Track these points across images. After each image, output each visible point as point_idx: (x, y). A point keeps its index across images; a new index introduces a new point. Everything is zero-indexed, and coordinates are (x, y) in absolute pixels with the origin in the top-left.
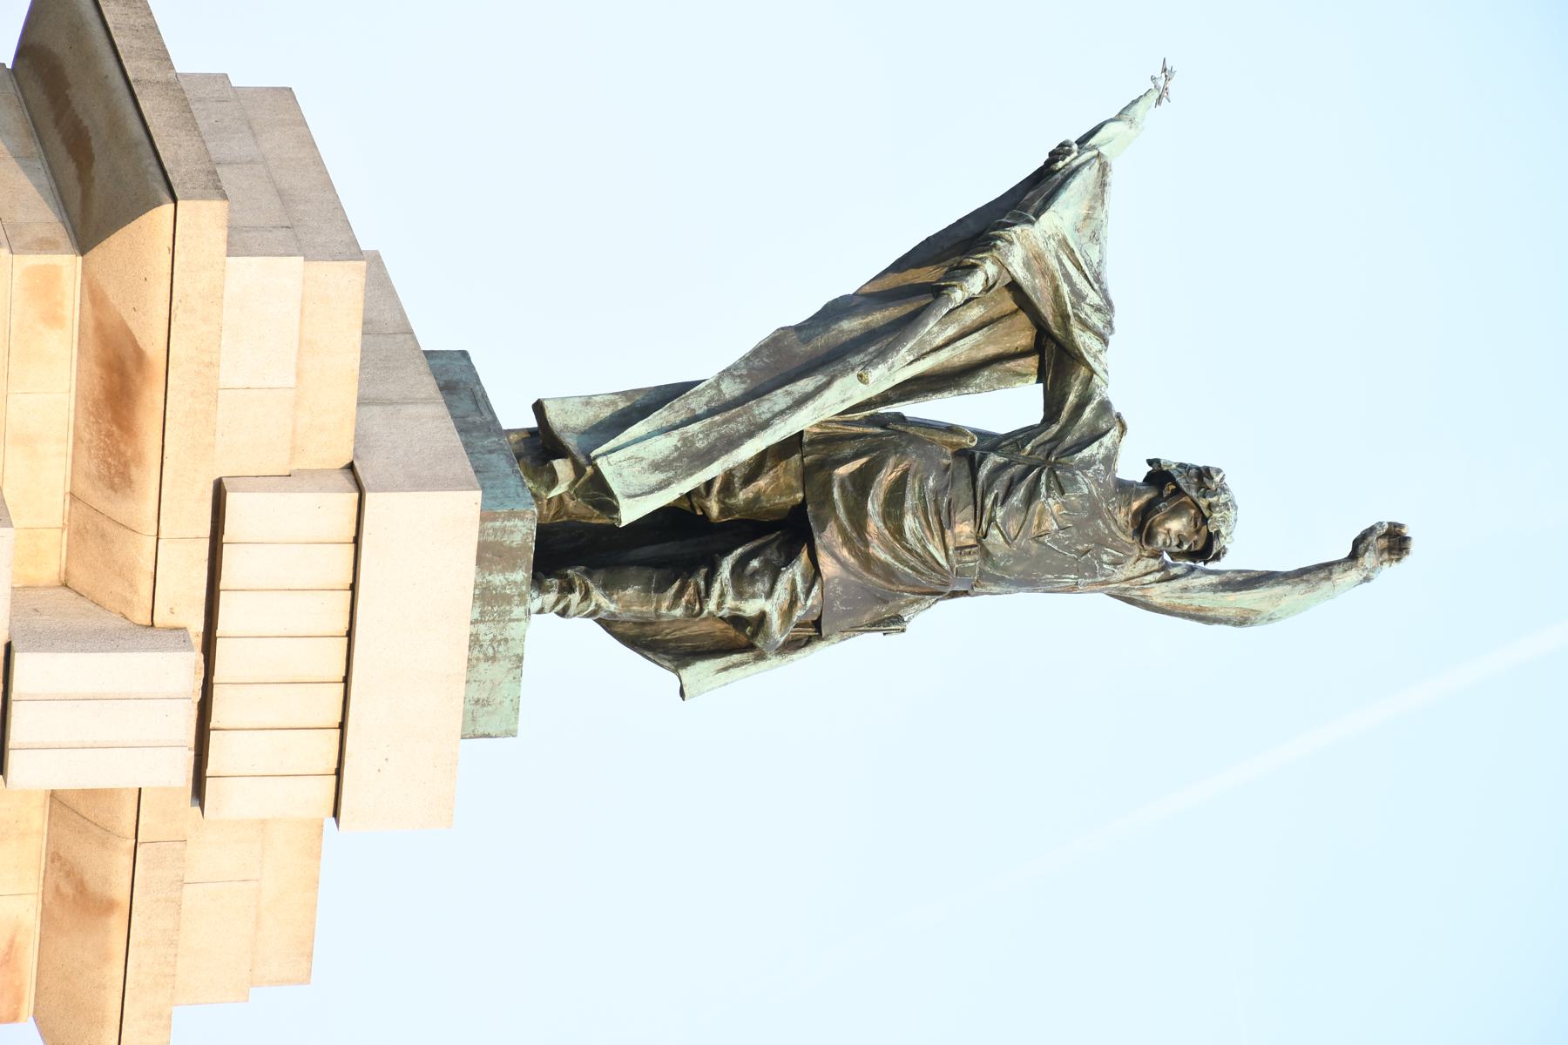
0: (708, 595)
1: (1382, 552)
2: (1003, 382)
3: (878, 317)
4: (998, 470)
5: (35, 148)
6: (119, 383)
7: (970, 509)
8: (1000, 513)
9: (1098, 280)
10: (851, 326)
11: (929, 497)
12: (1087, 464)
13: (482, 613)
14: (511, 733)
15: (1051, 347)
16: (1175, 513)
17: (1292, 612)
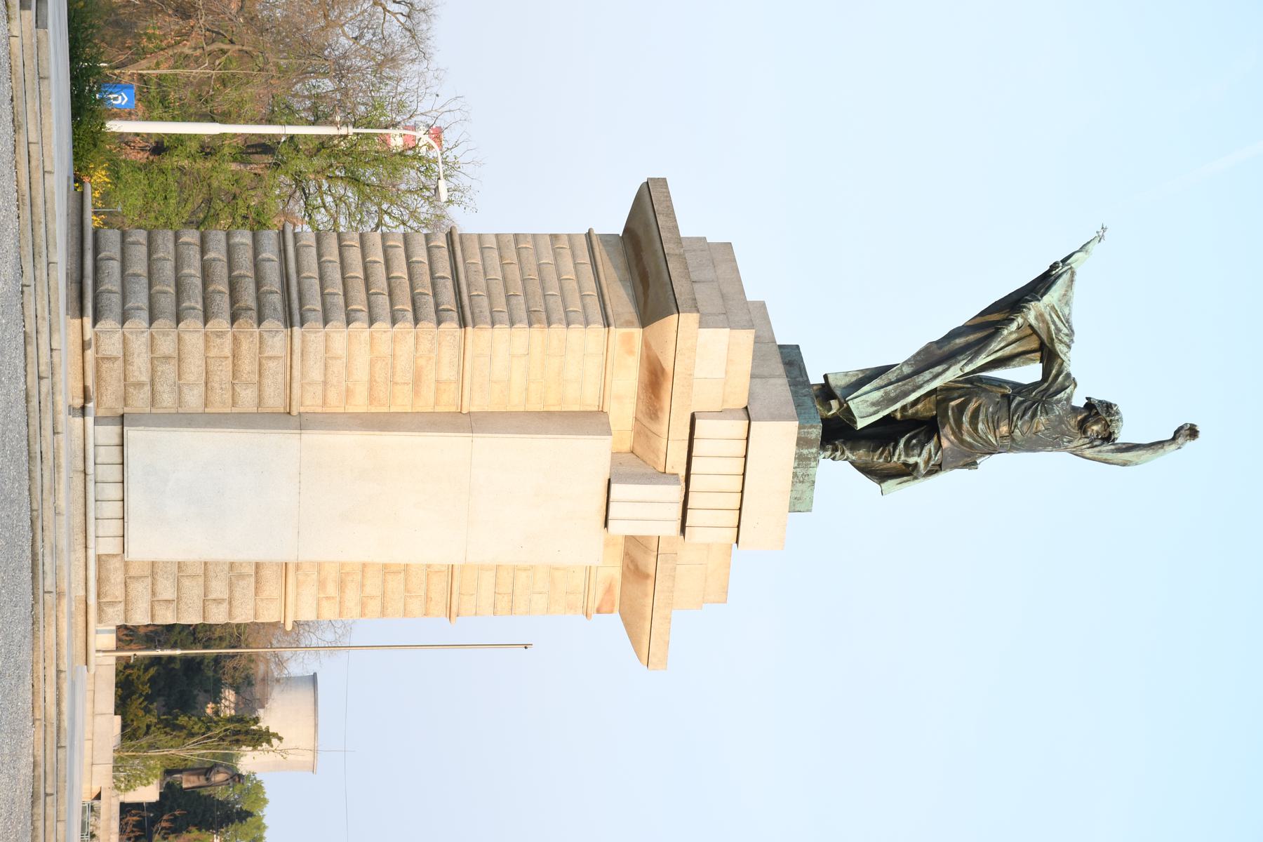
2: (1024, 363)
3: (972, 338)
4: (1020, 403)
5: (628, 276)
8: (1019, 423)
10: (960, 341)
12: (1059, 401)
14: (810, 511)
16: (1096, 423)
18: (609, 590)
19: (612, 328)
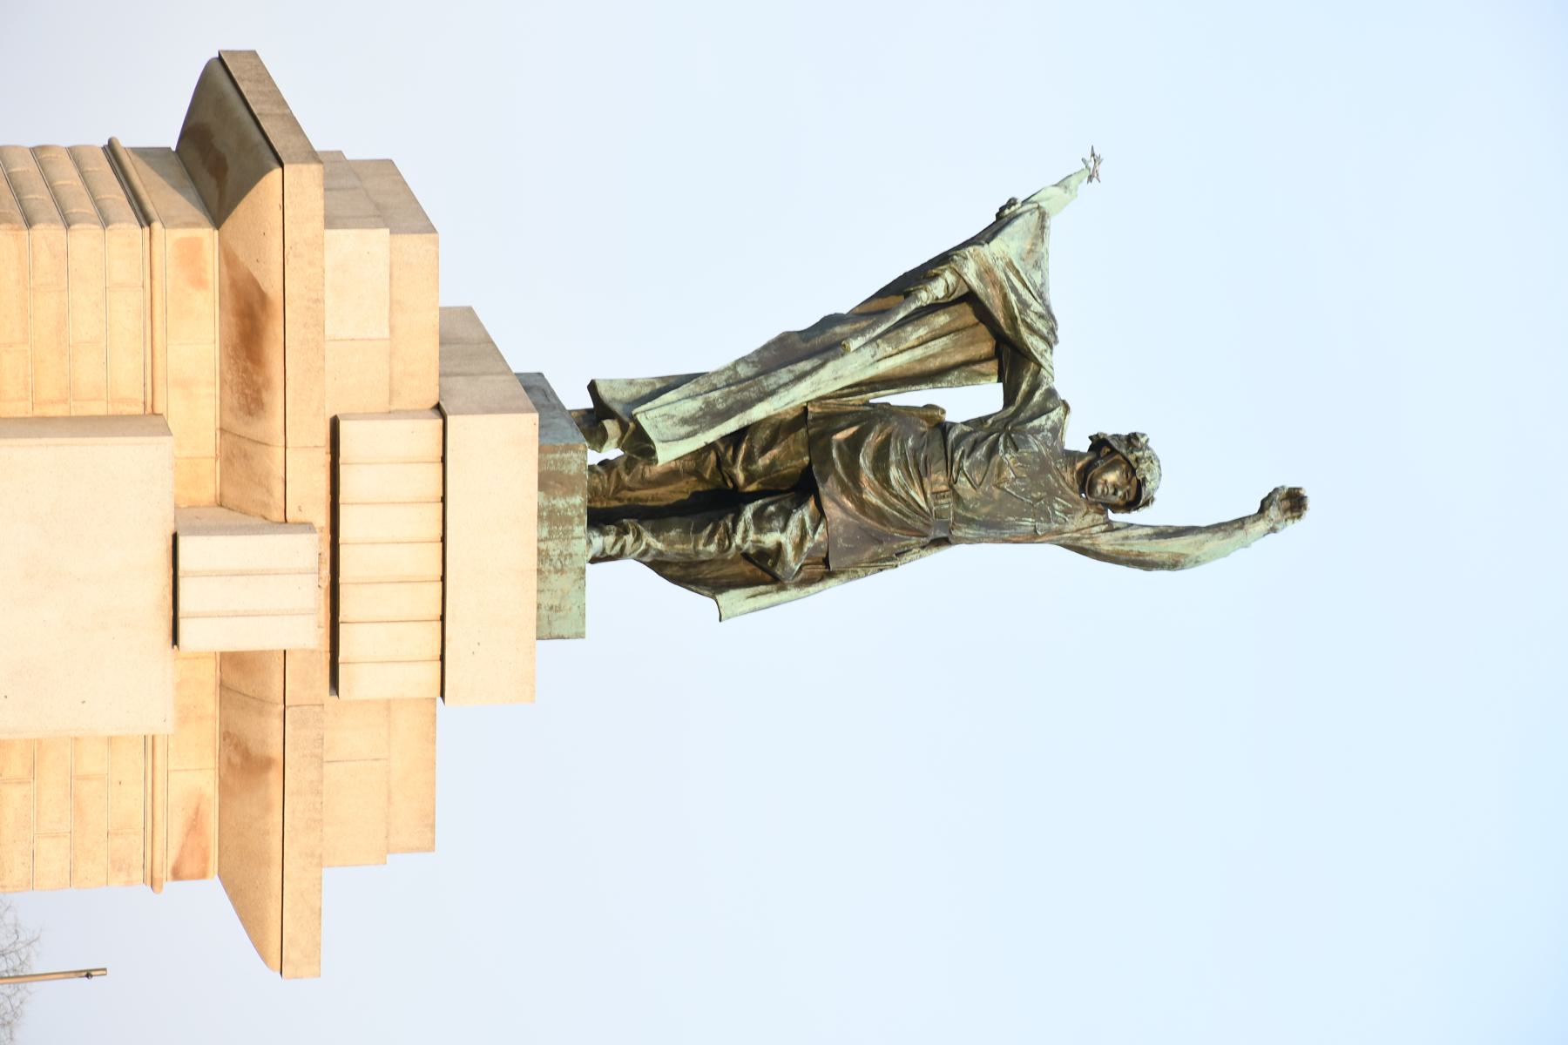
0: (734, 531)
1: (1285, 511)
5: (188, 183)
6: (250, 322)
7: (942, 463)
8: (966, 464)
9: (1041, 296)
12: (1038, 430)
13: (550, 532)
15: (1007, 350)
16: (1110, 467)
17: (1214, 556)
18: (195, 825)
19: (157, 225)
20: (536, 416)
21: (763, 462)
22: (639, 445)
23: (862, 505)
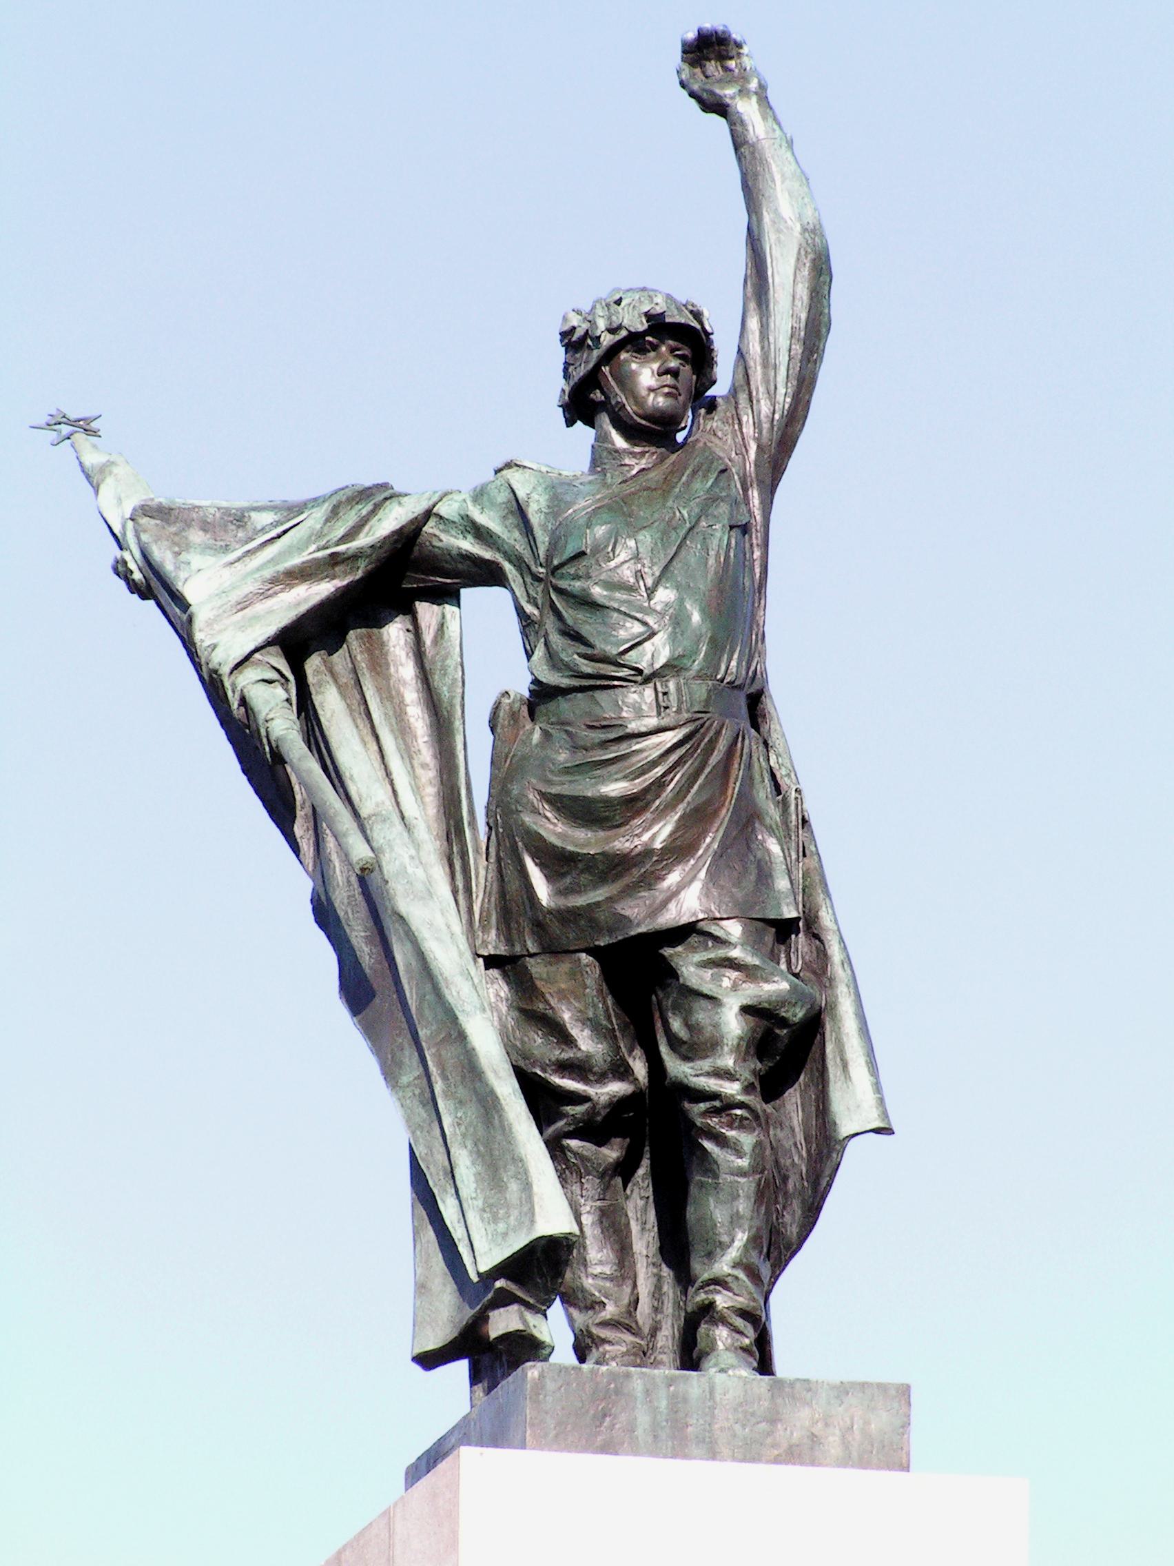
0: (715, 1096)
11: (581, 757)
16: (626, 381)
20: (462, 1448)
21: (587, 1043)
22: (541, 1268)
23: (679, 850)
